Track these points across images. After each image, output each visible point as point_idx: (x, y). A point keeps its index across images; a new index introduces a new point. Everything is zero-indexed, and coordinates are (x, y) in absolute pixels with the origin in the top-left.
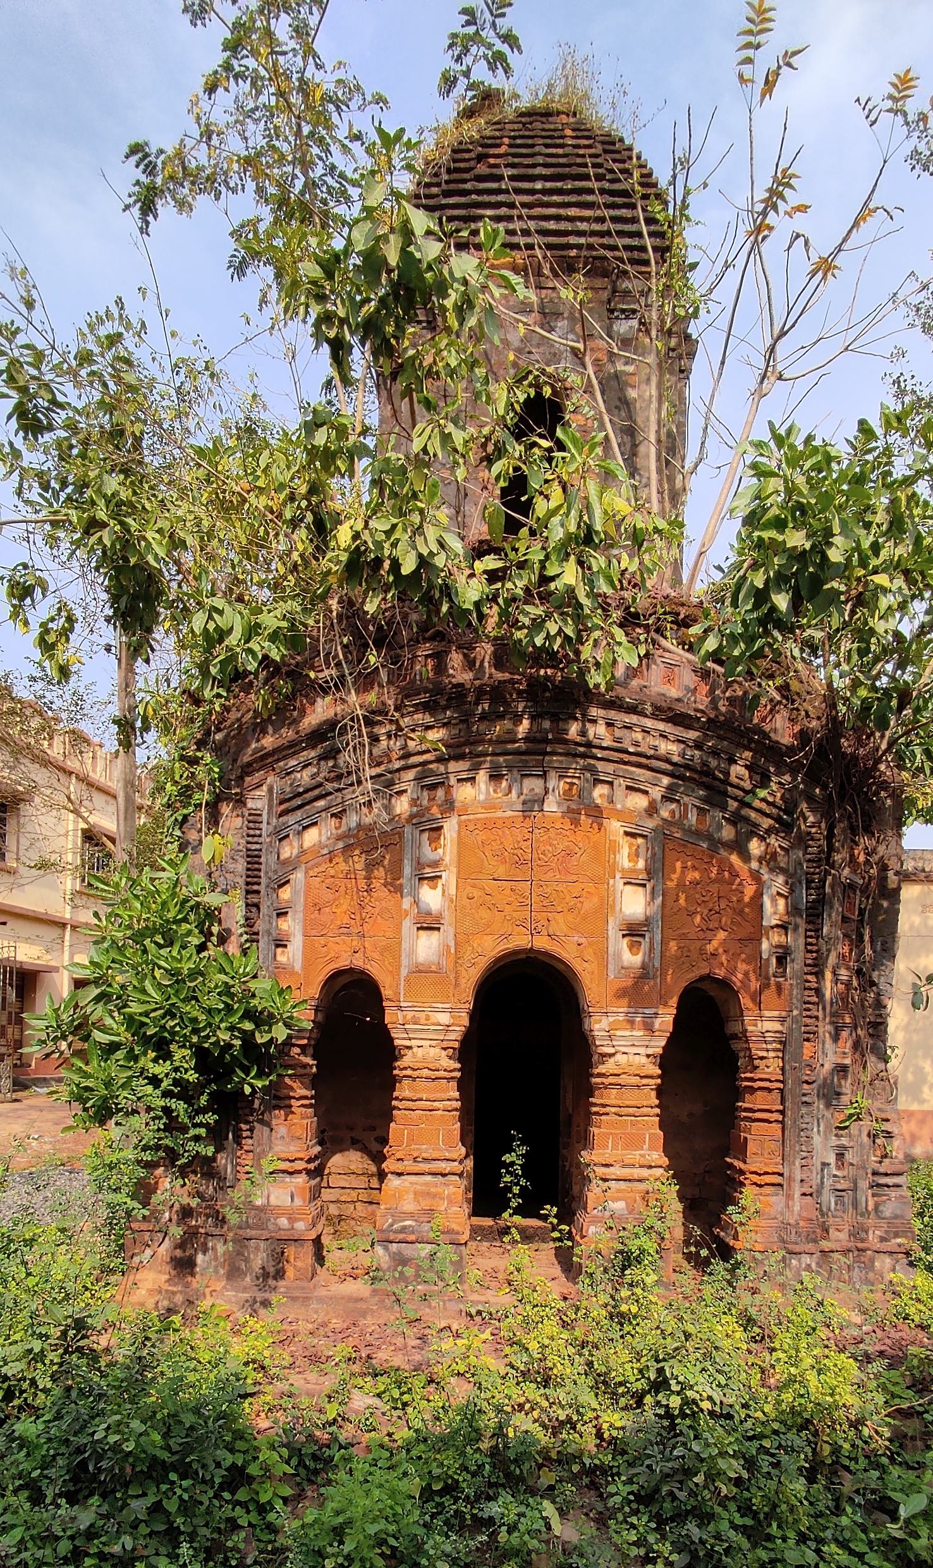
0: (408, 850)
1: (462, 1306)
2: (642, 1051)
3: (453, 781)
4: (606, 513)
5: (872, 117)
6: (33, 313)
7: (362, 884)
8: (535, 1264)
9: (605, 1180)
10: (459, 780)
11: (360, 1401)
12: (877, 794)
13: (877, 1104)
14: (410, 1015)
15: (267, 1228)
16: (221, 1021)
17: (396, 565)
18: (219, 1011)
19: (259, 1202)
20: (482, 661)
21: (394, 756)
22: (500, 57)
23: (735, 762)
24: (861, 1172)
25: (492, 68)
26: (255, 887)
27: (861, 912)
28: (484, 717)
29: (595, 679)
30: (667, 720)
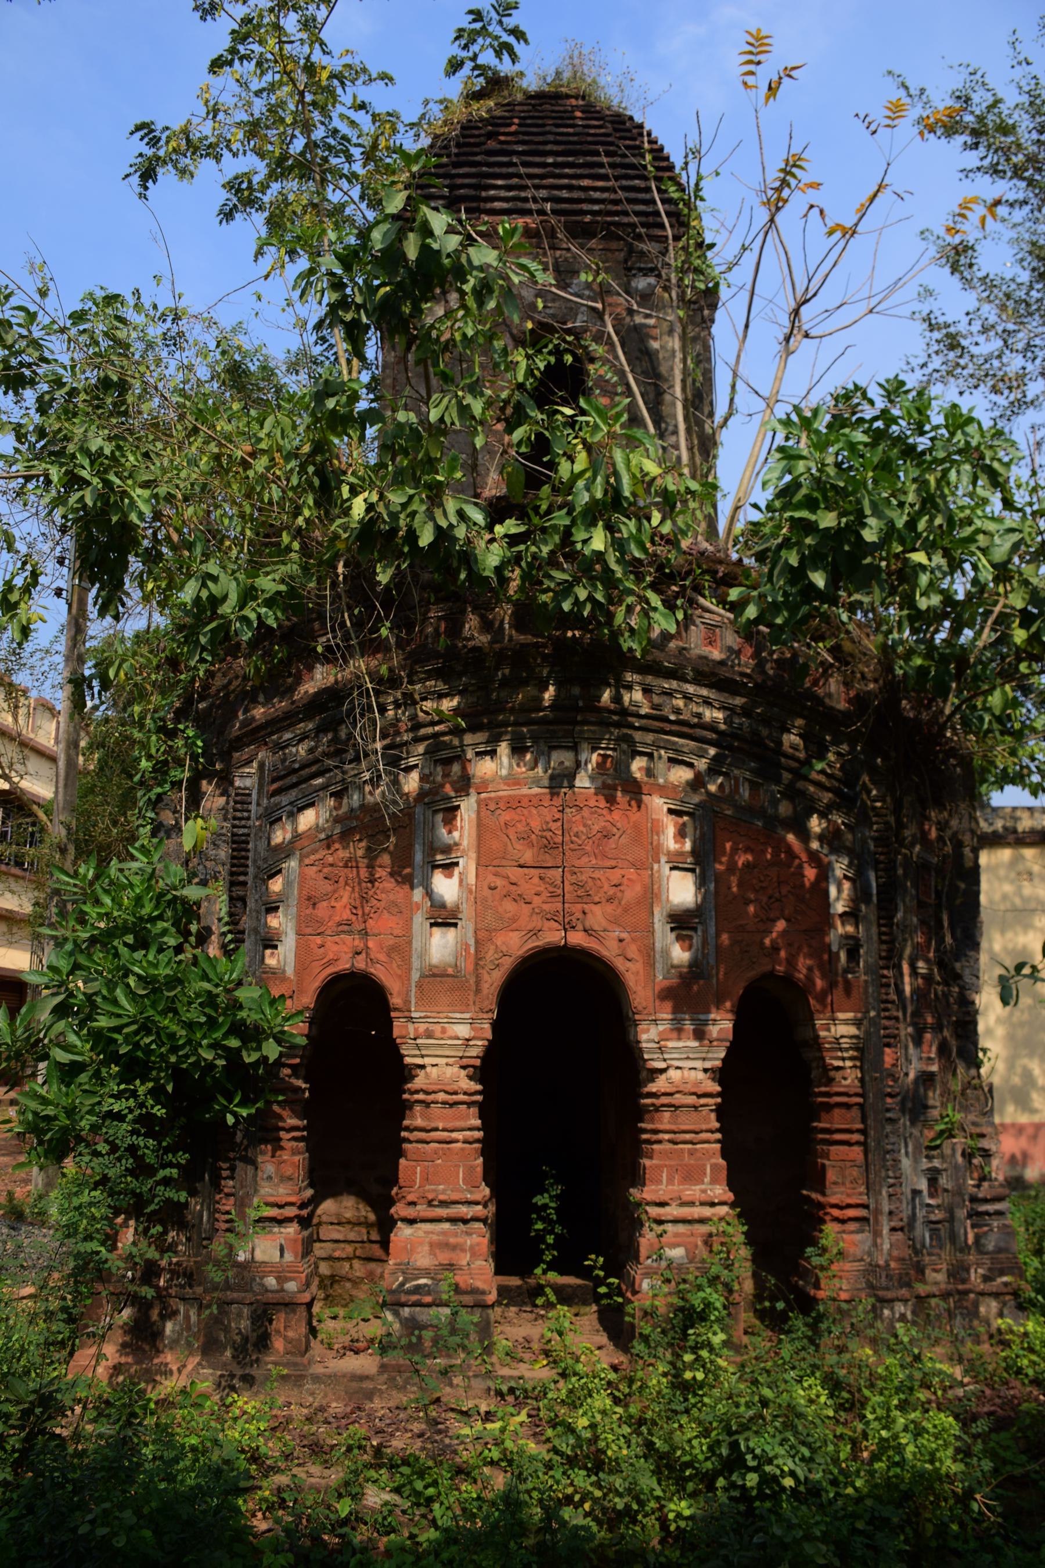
0: (419, 833)
1: (491, 1384)
2: (699, 1064)
3: (470, 754)
4: (634, 476)
5: (873, 128)
6: (47, 300)
7: (364, 873)
8: (583, 1335)
9: (660, 1222)
10: (478, 754)
11: (375, 1497)
12: (944, 762)
13: (971, 1117)
14: (422, 1028)
15: (251, 1290)
16: (204, 1037)
17: (412, 536)
18: (201, 1025)
19: (242, 1257)
20: (502, 622)
21: (403, 727)
22: (509, 48)
23: (789, 731)
24: (957, 1199)
25: (498, 54)
26: (242, 878)
27: (938, 894)
28: (505, 683)
29: (627, 643)
30: (709, 686)
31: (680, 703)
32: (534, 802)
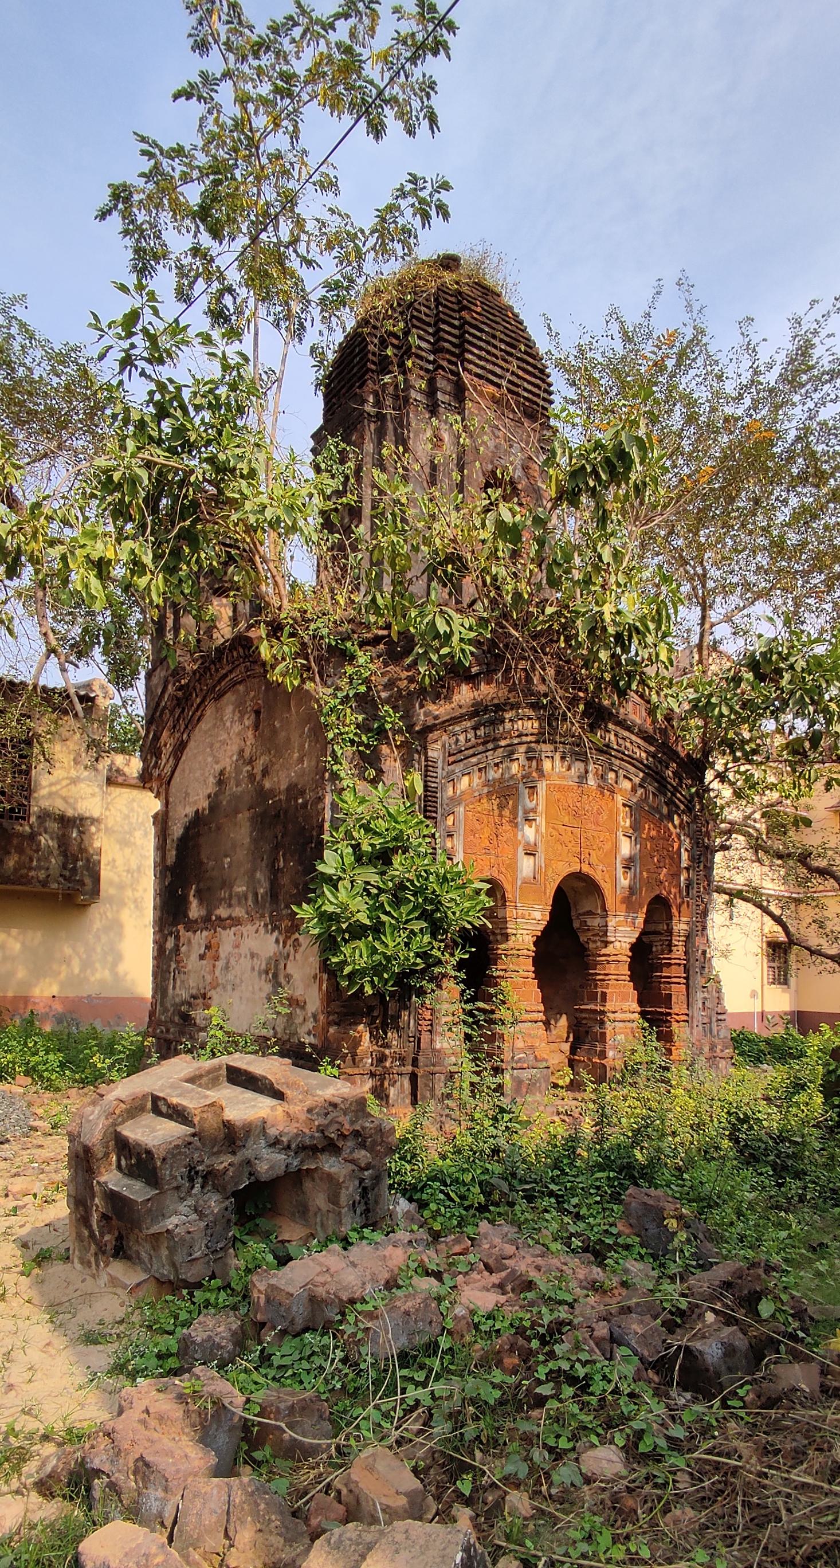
14: (520, 912)
31: (628, 745)
32: (569, 788)
